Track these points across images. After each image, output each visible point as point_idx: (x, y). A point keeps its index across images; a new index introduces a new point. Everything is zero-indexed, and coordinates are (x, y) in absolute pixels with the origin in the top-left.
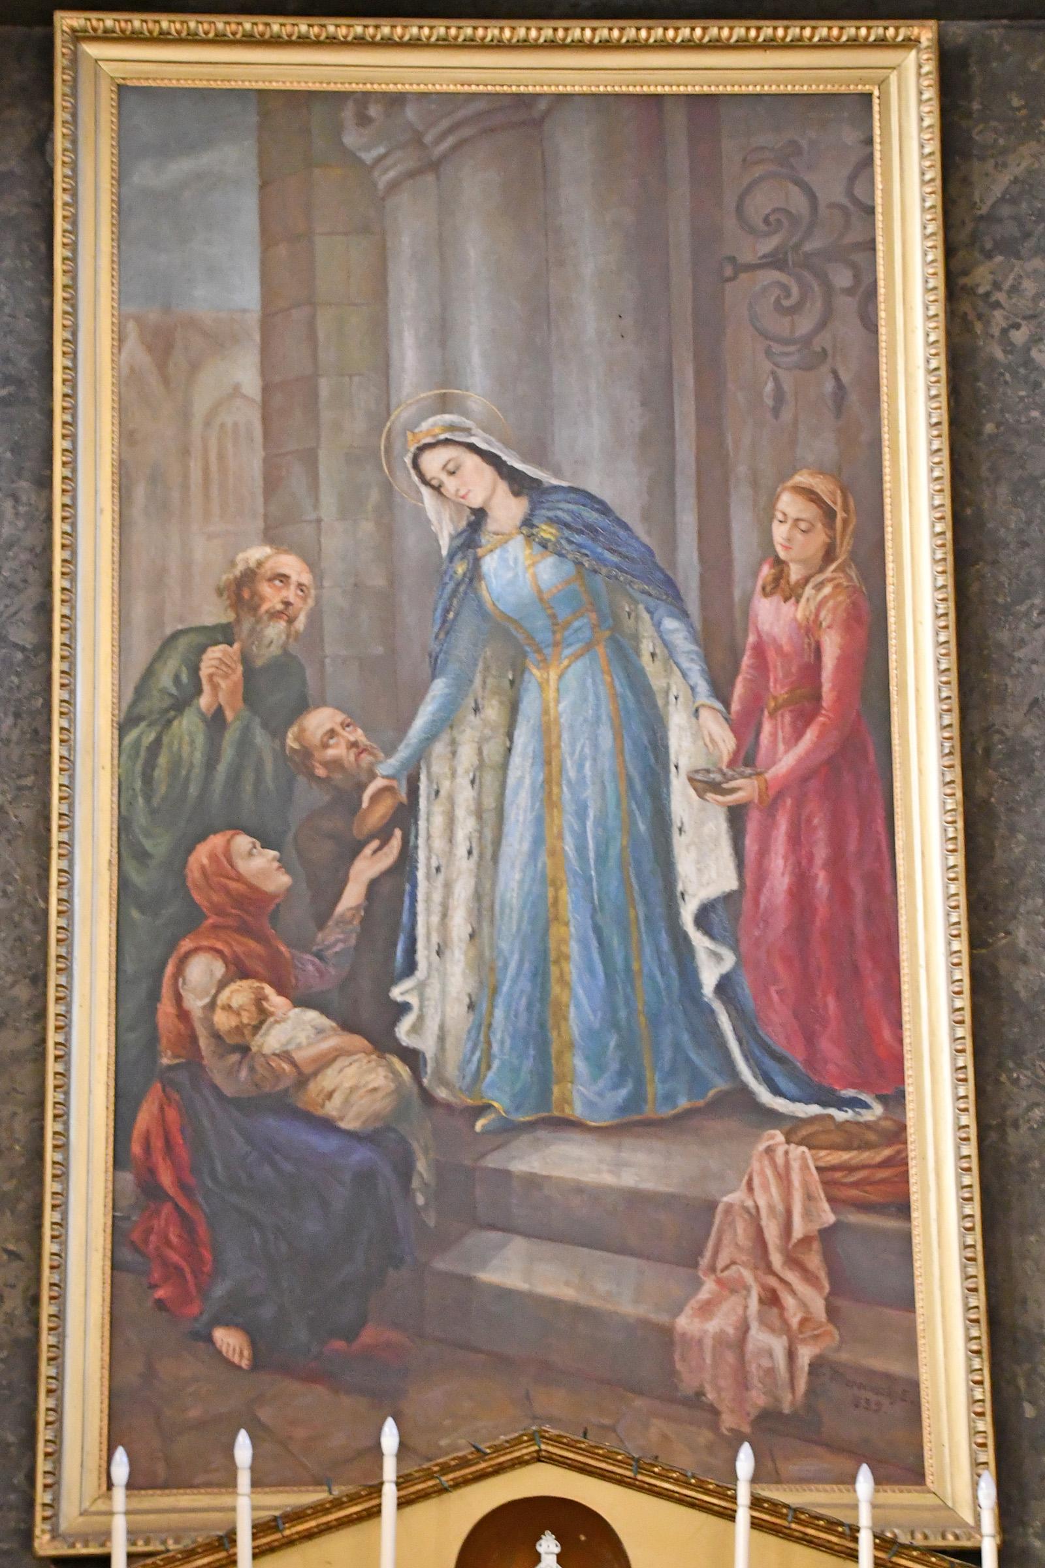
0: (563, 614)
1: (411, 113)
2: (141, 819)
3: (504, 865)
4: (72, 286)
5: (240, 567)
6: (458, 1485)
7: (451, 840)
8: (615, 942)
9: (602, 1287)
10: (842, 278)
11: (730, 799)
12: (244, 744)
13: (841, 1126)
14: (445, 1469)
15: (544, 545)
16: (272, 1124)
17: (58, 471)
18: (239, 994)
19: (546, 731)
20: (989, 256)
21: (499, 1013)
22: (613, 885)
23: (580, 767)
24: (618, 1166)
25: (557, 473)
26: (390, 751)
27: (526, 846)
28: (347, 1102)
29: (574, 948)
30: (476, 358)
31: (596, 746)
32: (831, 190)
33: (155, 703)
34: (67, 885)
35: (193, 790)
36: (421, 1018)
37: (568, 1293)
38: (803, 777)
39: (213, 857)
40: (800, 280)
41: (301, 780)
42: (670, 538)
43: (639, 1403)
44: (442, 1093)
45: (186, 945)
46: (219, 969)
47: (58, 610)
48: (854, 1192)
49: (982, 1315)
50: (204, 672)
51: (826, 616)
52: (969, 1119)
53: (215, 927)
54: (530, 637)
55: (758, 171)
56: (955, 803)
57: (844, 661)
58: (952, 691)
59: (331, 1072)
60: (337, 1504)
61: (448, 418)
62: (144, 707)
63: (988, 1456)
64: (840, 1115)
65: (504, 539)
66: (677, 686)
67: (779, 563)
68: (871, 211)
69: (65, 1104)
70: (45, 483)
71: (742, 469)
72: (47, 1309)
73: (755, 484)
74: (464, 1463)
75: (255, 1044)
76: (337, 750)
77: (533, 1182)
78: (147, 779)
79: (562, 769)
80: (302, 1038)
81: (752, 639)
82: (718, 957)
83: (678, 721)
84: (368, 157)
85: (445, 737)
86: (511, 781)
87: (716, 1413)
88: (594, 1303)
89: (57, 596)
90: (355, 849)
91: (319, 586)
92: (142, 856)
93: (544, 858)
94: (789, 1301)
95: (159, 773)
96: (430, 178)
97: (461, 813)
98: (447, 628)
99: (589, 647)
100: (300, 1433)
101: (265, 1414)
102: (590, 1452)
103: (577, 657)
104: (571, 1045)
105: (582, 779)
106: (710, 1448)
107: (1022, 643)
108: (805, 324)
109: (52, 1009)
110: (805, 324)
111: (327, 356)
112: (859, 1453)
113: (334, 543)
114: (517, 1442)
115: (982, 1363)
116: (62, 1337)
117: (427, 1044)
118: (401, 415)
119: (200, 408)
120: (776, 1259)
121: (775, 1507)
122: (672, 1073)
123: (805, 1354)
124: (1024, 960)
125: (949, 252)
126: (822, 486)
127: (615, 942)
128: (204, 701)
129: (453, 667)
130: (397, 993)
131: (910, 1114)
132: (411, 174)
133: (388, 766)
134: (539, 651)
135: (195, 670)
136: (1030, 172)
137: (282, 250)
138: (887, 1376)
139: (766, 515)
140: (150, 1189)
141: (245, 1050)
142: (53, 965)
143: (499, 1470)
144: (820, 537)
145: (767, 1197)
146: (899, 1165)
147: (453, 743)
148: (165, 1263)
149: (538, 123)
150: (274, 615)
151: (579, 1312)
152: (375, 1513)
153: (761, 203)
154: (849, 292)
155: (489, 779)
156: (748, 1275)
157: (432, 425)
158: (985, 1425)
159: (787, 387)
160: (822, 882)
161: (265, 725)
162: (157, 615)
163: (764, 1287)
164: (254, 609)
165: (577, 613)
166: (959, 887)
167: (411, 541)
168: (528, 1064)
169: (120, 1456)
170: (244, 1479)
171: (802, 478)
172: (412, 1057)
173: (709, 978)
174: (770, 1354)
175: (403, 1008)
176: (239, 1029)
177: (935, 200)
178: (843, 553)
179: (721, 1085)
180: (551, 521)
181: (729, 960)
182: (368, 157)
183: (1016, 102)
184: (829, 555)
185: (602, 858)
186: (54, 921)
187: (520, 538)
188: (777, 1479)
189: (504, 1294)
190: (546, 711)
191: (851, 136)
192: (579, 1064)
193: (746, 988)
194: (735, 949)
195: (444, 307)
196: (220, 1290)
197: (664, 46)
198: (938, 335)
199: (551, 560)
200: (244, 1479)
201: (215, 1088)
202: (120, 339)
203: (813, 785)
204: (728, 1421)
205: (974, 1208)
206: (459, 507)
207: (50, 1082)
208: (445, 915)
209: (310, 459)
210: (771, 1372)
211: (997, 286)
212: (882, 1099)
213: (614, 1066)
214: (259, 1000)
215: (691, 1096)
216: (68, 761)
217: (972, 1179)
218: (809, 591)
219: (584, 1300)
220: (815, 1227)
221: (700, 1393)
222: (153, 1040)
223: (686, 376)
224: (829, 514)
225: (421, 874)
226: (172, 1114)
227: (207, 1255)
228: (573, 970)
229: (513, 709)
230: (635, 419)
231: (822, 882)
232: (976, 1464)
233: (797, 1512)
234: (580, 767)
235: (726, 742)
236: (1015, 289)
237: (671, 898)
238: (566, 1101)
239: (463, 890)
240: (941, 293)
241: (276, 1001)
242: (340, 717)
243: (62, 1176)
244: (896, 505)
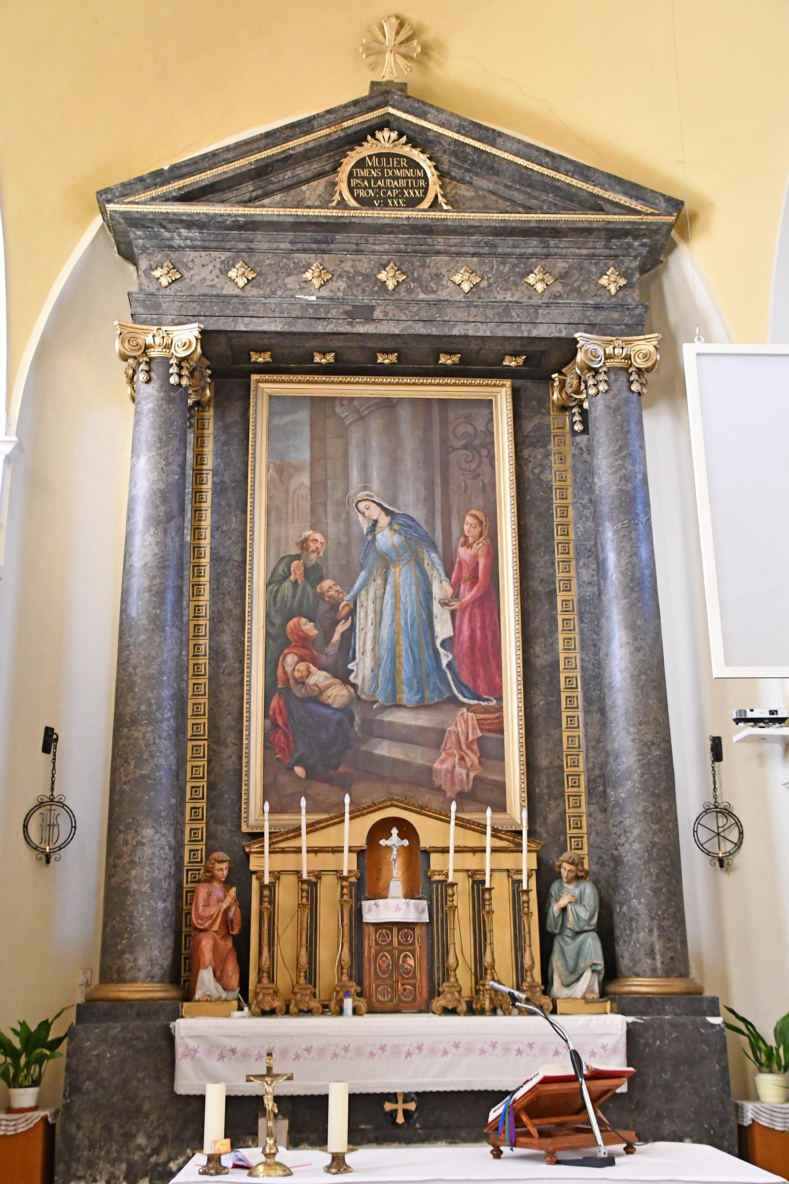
0: (401, 552)
1: (356, 403)
2: (273, 613)
3: (382, 627)
4: (254, 454)
5: (303, 537)
6: (367, 813)
7: (366, 620)
8: (416, 651)
9: (411, 755)
10: (484, 452)
11: (451, 608)
12: (304, 589)
13: (483, 707)
14: (364, 809)
15: (395, 531)
16: (312, 706)
17: (249, 508)
18: (302, 666)
19: (396, 587)
20: (528, 447)
21: (381, 673)
22: (415, 634)
23: (406, 598)
24: (416, 719)
25: (399, 509)
26: (348, 593)
27: (389, 622)
28: (334, 699)
29: (404, 653)
30: (375, 475)
31: (411, 592)
32: (481, 426)
33: (277, 578)
34: (250, 633)
35: (288, 604)
36: (357, 674)
37: (401, 757)
38: (473, 602)
39: (294, 625)
40: (472, 454)
41: (321, 601)
42: (433, 531)
43: (422, 789)
44: (363, 697)
45: (286, 651)
46: (296, 659)
47: (248, 550)
48: (487, 727)
49: (524, 763)
50: (292, 569)
51: (480, 553)
52: (522, 705)
53: (295, 646)
54: (391, 559)
55: (459, 421)
56: (518, 610)
57: (485, 567)
58: (518, 576)
59: (330, 690)
60: (332, 819)
61: (366, 492)
62: (274, 579)
63: (525, 804)
64: (483, 704)
65: (383, 529)
66: (435, 574)
67: (466, 537)
68: (493, 433)
69: (250, 699)
70: (245, 512)
71: (454, 509)
72: (244, 760)
73: (459, 513)
74: (369, 807)
75: (307, 681)
76: (332, 593)
77: (391, 724)
78: (275, 601)
79: (400, 597)
80: (321, 680)
81: (458, 560)
82: (448, 656)
83: (435, 584)
84: (343, 416)
85: (365, 589)
86: (385, 602)
87: (445, 792)
88: (410, 760)
89: (248, 546)
90: (336, 623)
91: (327, 543)
92: (273, 624)
93: (394, 625)
94: (467, 759)
95: (278, 599)
96: (361, 422)
97: (369, 612)
98: (366, 555)
99: (408, 562)
100: (320, 798)
101: (310, 792)
102: (407, 804)
103: (405, 565)
104: (402, 682)
105: (406, 602)
106: (443, 802)
107: (538, 562)
108: (474, 466)
109: (246, 670)
110: (474, 466)
111: (330, 474)
112: (488, 803)
113: (332, 529)
114: (386, 801)
115: (524, 777)
116: (249, 769)
117: (359, 682)
118: (352, 492)
119: (292, 489)
120: (464, 747)
121: (462, 820)
122: (433, 691)
123: (472, 775)
124: (538, 657)
125: (516, 446)
126: (479, 514)
127: (416, 651)
128: (292, 577)
129: (368, 567)
130: (350, 666)
131: (504, 703)
132: (356, 421)
133: (348, 597)
134: (393, 563)
135: (289, 568)
136: (539, 423)
137: (317, 443)
138: (497, 781)
139: (462, 522)
140: (275, 725)
141: (304, 683)
142: (246, 657)
143: (380, 809)
144: (478, 529)
145: (461, 728)
146: (501, 719)
147: (367, 590)
148: (280, 747)
149: (394, 406)
150: (313, 551)
151: (404, 763)
152: (343, 821)
153: (461, 430)
154: (487, 457)
155: (378, 602)
156: (455, 751)
157: (361, 495)
158: (525, 795)
159: (468, 484)
160: (478, 633)
161: (310, 585)
162: (278, 552)
163: (460, 755)
164: (307, 550)
165: (405, 552)
166: (519, 635)
167: (355, 529)
168: (389, 688)
169: (267, 804)
170: (303, 811)
171: (473, 512)
172: (354, 686)
173: (444, 662)
174: (462, 775)
175: (352, 671)
176: (302, 677)
177: (512, 430)
178: (485, 533)
179: (448, 694)
180: (397, 524)
181: (451, 657)
182: (343, 416)
183: (535, 403)
184: (481, 535)
185: (412, 626)
186: (246, 644)
187: (388, 529)
188: (463, 811)
189: (382, 757)
190: (395, 581)
191: (486, 411)
192: (405, 688)
193: (455, 665)
194: (452, 653)
195: (366, 459)
196: (296, 755)
197: (431, 384)
198: (513, 470)
199: (397, 535)
200: (303, 811)
201: (295, 695)
202: (268, 469)
203: (476, 603)
204: (449, 794)
205: (523, 731)
206: (369, 519)
207: (245, 692)
208: (364, 643)
209: (325, 504)
210: (462, 780)
211: (530, 456)
212: (496, 699)
213: (416, 689)
214: (308, 668)
215: (439, 698)
216: (251, 595)
217: (522, 722)
218: (475, 545)
219: (406, 759)
220: (475, 737)
221: (440, 787)
222: (276, 679)
223: (438, 480)
224: (481, 523)
225: (357, 630)
226: (281, 702)
227: (292, 744)
228: (403, 660)
229: (386, 581)
230: (423, 493)
231: (478, 633)
232: (522, 806)
233: (468, 821)
234: (406, 598)
235: (450, 591)
236: (535, 457)
237: (433, 638)
238: (401, 699)
239: (370, 635)
240: (514, 457)
241: (313, 669)
242: (333, 582)
243: (249, 721)
244: (501, 522)
